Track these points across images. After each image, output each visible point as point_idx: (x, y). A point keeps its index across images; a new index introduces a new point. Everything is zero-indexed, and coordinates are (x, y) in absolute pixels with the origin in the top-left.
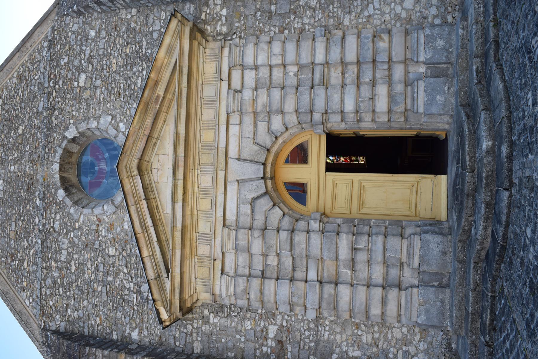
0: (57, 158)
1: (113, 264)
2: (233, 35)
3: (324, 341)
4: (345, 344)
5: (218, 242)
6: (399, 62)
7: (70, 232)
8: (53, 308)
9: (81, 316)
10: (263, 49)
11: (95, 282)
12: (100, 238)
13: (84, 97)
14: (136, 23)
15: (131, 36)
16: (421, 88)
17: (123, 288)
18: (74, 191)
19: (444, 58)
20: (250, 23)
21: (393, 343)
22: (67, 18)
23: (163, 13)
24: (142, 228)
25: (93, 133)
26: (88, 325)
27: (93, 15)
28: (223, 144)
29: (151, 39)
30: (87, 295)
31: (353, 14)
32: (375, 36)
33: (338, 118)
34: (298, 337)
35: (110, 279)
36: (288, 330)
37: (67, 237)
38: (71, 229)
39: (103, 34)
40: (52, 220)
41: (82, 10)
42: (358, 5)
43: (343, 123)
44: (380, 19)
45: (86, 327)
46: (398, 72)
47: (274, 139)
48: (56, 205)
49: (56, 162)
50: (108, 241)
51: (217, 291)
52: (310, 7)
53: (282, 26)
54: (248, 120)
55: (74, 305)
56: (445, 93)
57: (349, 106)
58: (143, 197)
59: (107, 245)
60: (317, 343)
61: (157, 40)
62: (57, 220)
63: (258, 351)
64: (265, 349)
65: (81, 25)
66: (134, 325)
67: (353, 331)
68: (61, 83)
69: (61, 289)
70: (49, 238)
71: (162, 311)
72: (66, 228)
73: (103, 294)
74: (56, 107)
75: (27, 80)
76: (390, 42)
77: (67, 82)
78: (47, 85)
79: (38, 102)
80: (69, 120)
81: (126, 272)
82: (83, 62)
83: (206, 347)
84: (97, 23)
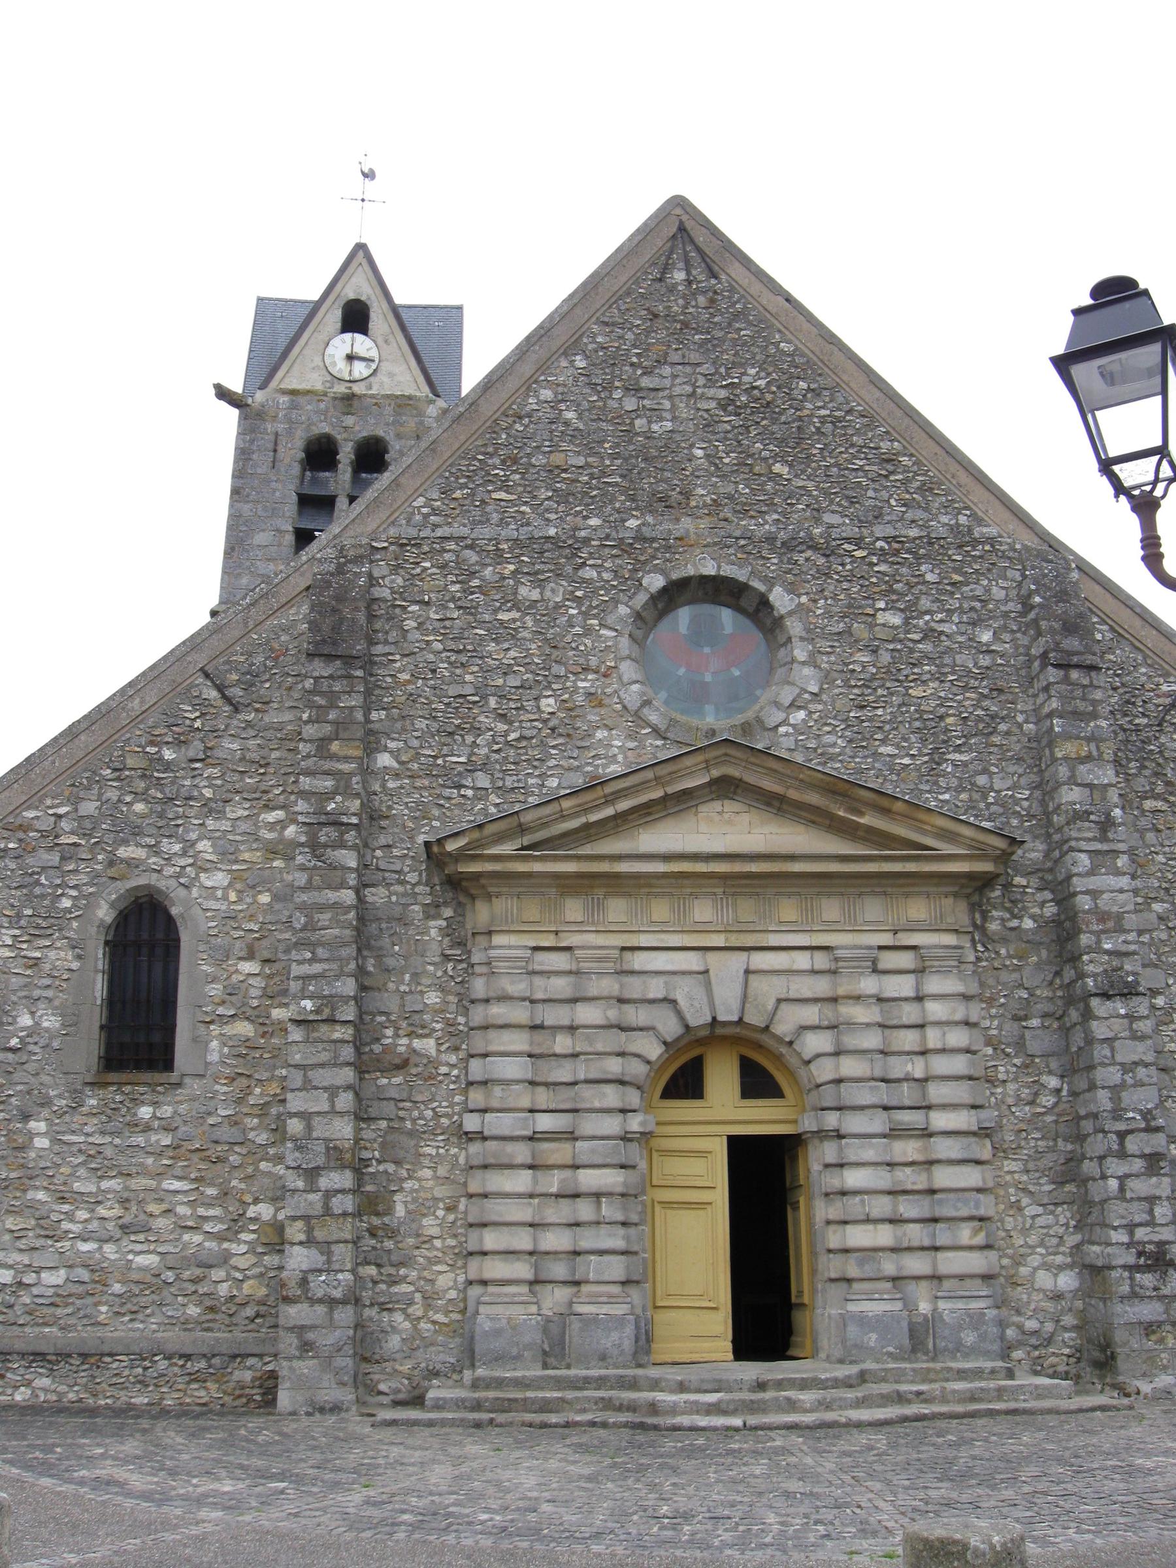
0: (728, 571)
1: (522, 708)
2: (984, 946)
3: (417, 1146)
4: (416, 1187)
5: (593, 939)
6: (935, 1265)
7: (579, 607)
8: (418, 570)
9: (410, 636)
10: (954, 1011)
11: (481, 668)
12: (572, 678)
13: (855, 625)
14: (1008, 733)
15: (981, 726)
16: (887, 1306)
17: (478, 731)
18: (660, 606)
19: (943, 1344)
20: (1005, 976)
21: (426, 1274)
22: (1018, 573)
23: (1027, 792)
24: (613, 793)
25: (782, 645)
26: (391, 654)
27: (1024, 633)
28: (774, 940)
29: (975, 771)
30: (452, 650)
31: (1025, 1178)
32: (981, 1219)
33: (831, 1157)
34: (419, 1098)
35: (492, 702)
36: (431, 1077)
37: (568, 600)
38: (583, 609)
39: (985, 661)
40: (600, 562)
41: (1032, 615)
42: (1041, 1185)
43: (820, 1168)
44: (1014, 1229)
45: (387, 649)
46: (916, 1264)
47: (787, 1039)
48: (630, 571)
49: (719, 567)
50: (567, 696)
51: (497, 940)
52: (1036, 1094)
53: (1000, 1042)
54: (821, 986)
55: (428, 618)
56: (883, 1347)
57: (854, 1178)
58: (670, 790)
59: (559, 693)
60: (411, 1134)
61: (972, 784)
62: (599, 573)
63: (384, 1018)
64: (389, 1032)
65: (1003, 608)
66: (404, 758)
67: (441, 1200)
68: (883, 568)
69: (457, 587)
70: (561, 556)
71: (461, 842)
72: (585, 596)
73: (459, 687)
74: (832, 559)
75: (886, 477)
76: (971, 1248)
77: (886, 582)
78: (879, 531)
79: (840, 510)
80: (807, 594)
81: (509, 738)
82: (927, 618)
83: (380, 914)
84: (1007, 646)
